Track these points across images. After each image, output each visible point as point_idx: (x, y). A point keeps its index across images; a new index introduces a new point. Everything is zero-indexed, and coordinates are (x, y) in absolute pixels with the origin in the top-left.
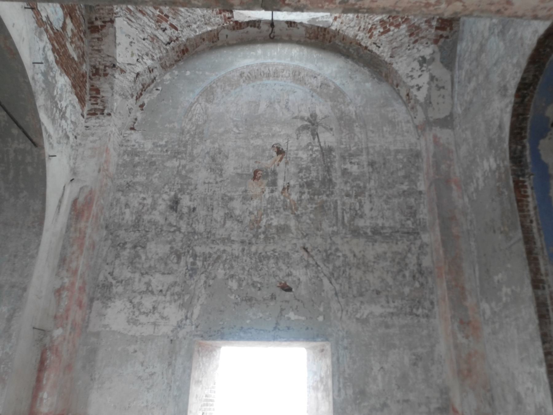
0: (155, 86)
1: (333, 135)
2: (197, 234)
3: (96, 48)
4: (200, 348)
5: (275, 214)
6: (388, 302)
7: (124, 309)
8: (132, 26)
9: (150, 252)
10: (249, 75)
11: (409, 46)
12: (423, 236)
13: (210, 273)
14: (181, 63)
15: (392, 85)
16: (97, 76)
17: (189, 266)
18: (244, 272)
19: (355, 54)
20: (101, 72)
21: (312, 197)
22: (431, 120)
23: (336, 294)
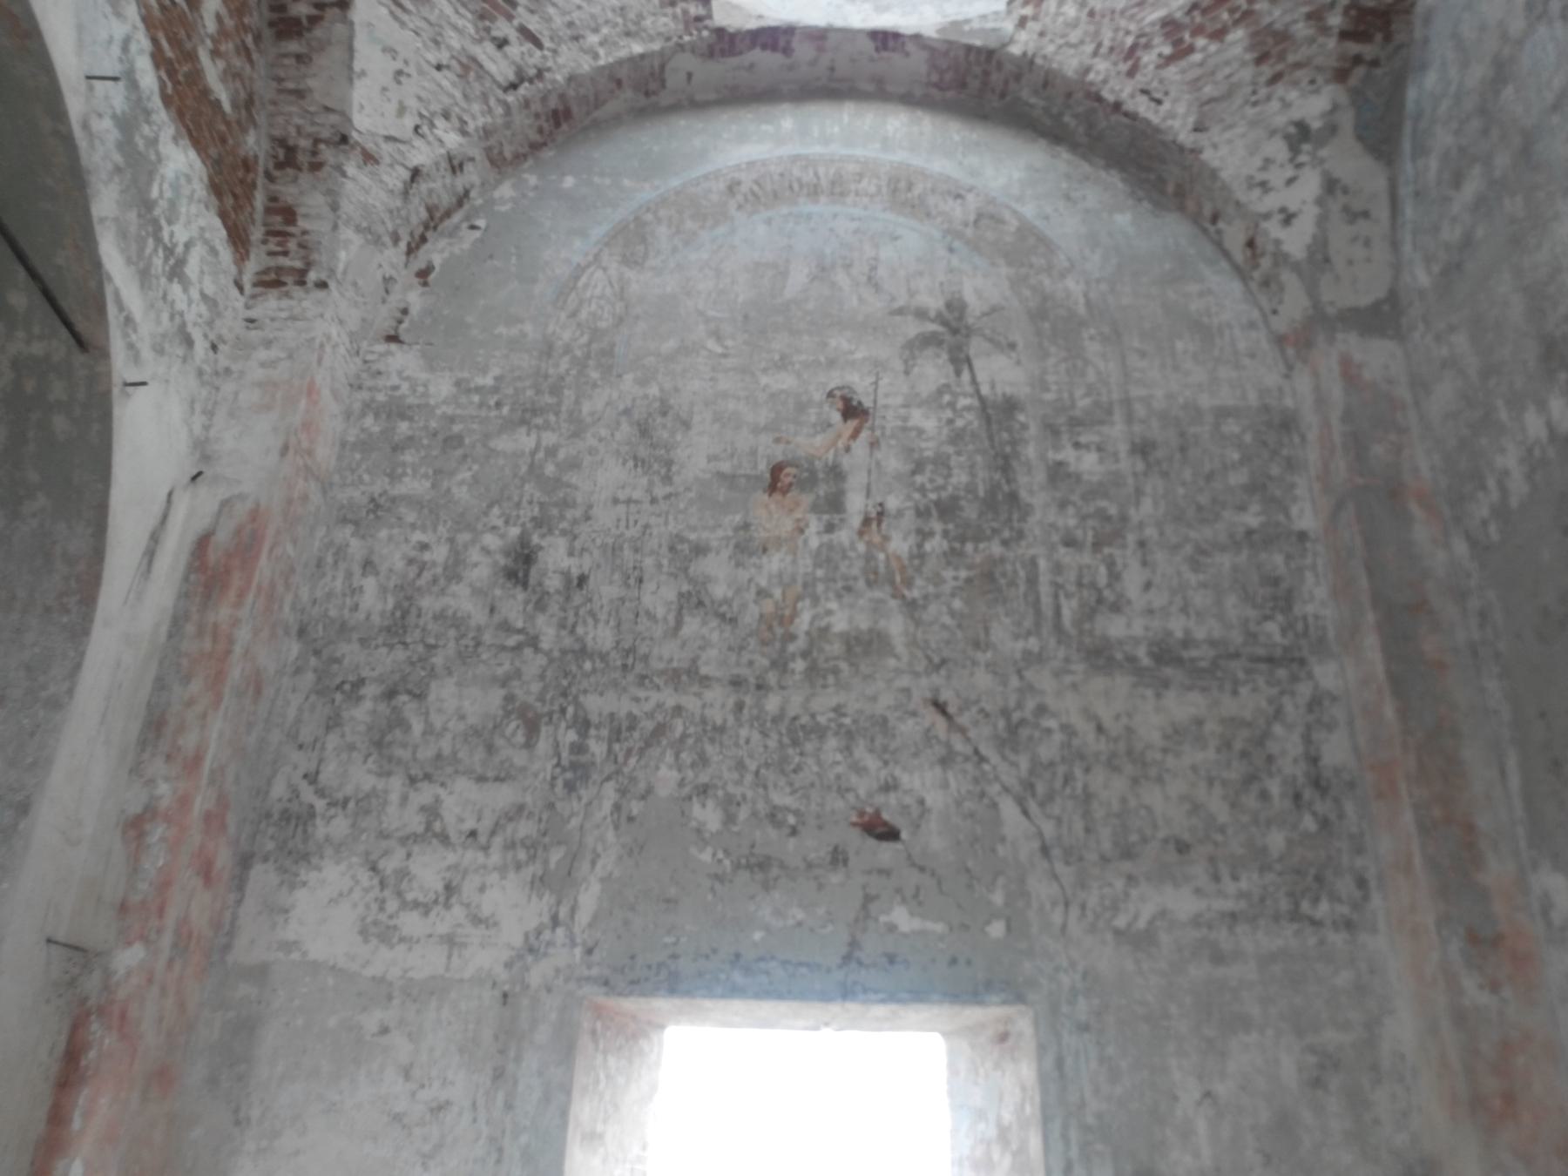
0: (467, 218)
1: (1018, 363)
2: (591, 657)
3: (290, 85)
4: (599, 1025)
5: (839, 596)
6: (1216, 878)
7: (351, 890)
8: (403, 24)
9: (440, 711)
10: (756, 188)
11: (1254, 92)
12: (1318, 670)
13: (633, 779)
14: (548, 154)
15: (1196, 219)
16: (290, 171)
17: (565, 754)
18: (742, 776)
19: (1081, 130)
20: (303, 159)
21: (957, 545)
22: (1330, 311)
23: (1045, 851)
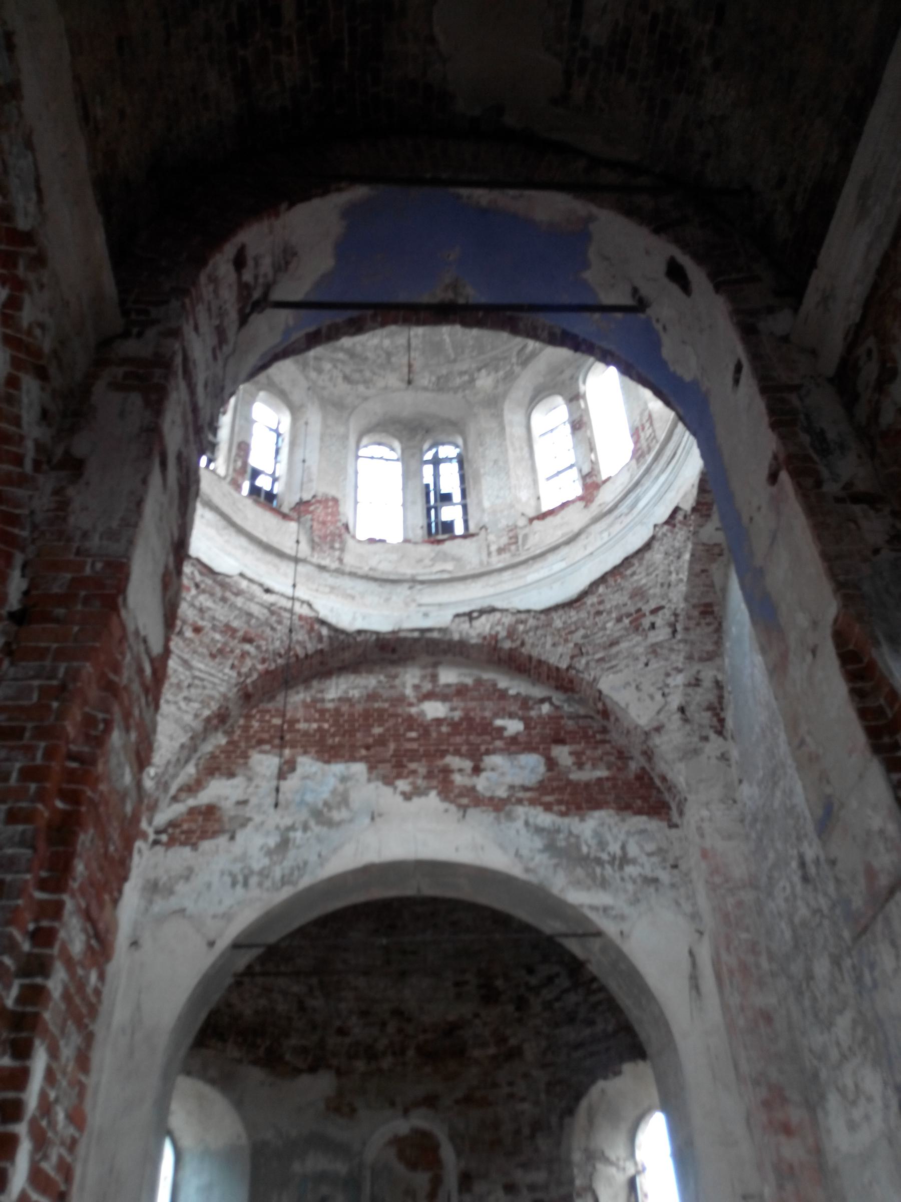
8: (621, 671)
